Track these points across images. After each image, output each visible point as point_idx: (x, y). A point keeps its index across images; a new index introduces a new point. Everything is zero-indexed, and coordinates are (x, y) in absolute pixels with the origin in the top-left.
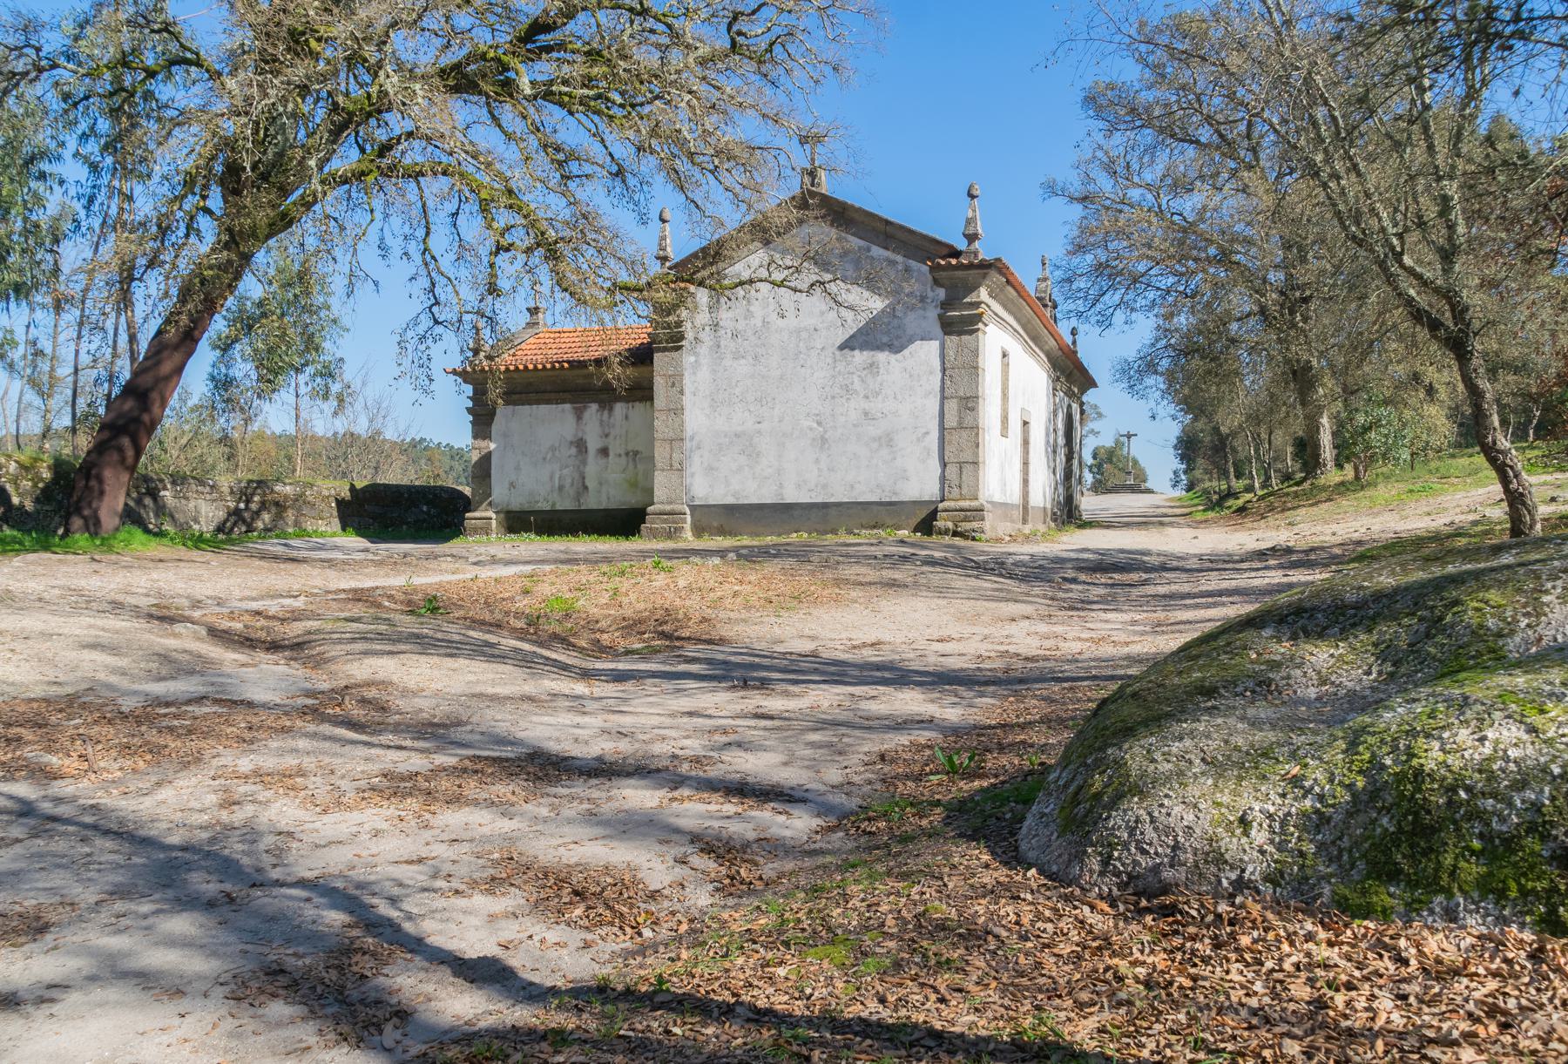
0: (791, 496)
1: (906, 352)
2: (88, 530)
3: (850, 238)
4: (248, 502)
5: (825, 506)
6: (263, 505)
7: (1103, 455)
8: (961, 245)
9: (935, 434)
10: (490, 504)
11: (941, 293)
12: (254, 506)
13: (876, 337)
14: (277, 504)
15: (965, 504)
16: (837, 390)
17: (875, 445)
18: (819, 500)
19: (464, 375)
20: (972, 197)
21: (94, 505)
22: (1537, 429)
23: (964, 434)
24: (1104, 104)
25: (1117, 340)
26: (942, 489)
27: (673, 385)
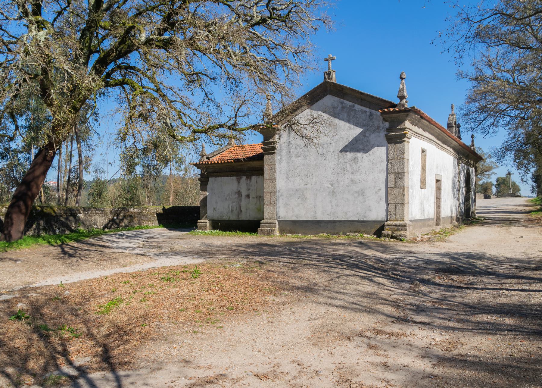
0: (320, 217)
1: (370, 152)
3: (345, 102)
4: (118, 216)
5: (334, 222)
6: (124, 217)
7: (500, 181)
8: (396, 101)
9: (384, 190)
10: (207, 217)
11: (387, 125)
12: (120, 218)
13: (356, 146)
14: (131, 216)
17: (356, 195)
18: (332, 219)
20: (402, 79)
21: (9, 229)
23: (397, 190)
25: (491, 141)
26: (387, 216)
27: (271, 169)
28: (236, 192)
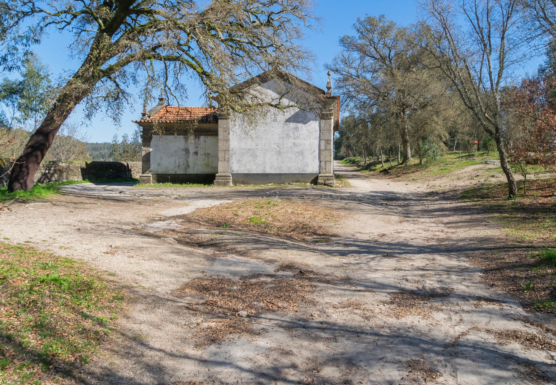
0: (268, 171)
1: (308, 124)
2: (22, 188)
4: (49, 170)
5: (280, 174)
6: (55, 171)
9: (317, 152)
12: (51, 172)
14: (60, 170)
15: (328, 175)
16: (284, 136)
17: (297, 155)
19: (140, 123)
21: (25, 178)
22: (456, 147)
23: (327, 152)
24: (344, 41)
26: (320, 170)
28: (183, 150)
